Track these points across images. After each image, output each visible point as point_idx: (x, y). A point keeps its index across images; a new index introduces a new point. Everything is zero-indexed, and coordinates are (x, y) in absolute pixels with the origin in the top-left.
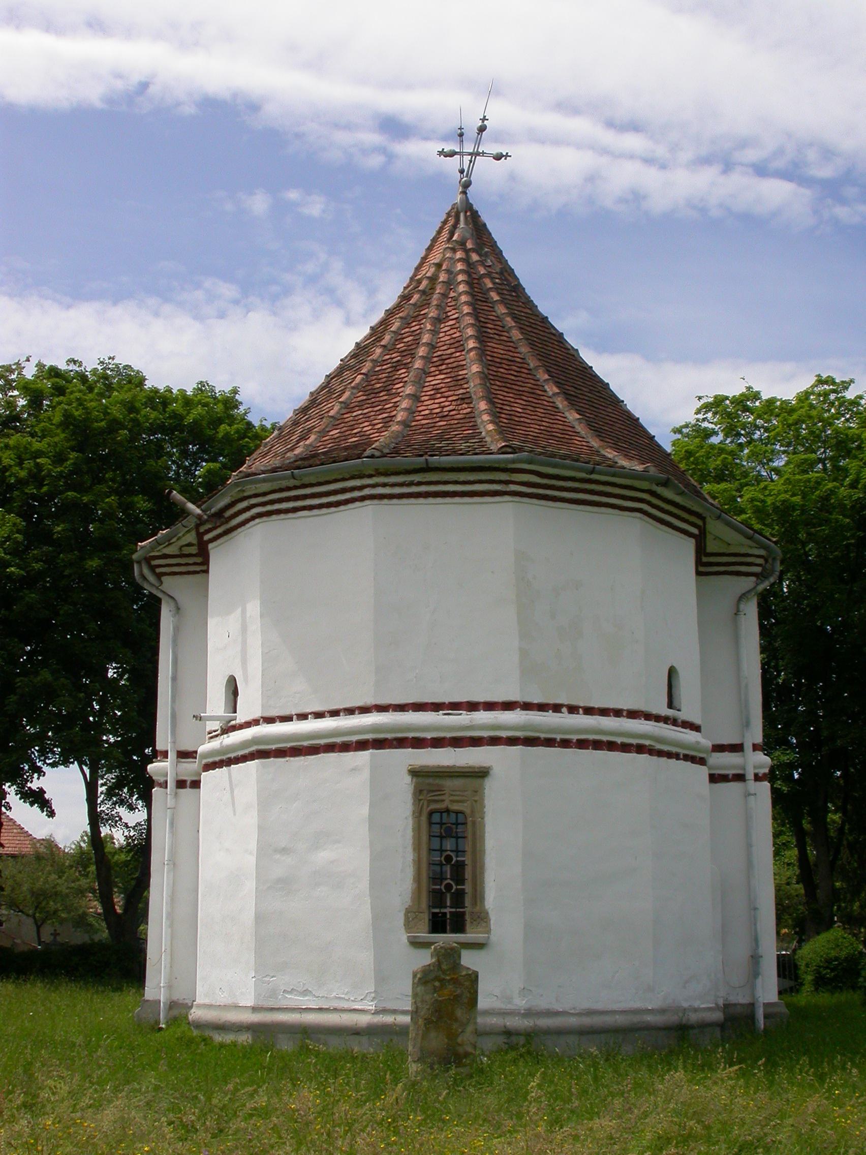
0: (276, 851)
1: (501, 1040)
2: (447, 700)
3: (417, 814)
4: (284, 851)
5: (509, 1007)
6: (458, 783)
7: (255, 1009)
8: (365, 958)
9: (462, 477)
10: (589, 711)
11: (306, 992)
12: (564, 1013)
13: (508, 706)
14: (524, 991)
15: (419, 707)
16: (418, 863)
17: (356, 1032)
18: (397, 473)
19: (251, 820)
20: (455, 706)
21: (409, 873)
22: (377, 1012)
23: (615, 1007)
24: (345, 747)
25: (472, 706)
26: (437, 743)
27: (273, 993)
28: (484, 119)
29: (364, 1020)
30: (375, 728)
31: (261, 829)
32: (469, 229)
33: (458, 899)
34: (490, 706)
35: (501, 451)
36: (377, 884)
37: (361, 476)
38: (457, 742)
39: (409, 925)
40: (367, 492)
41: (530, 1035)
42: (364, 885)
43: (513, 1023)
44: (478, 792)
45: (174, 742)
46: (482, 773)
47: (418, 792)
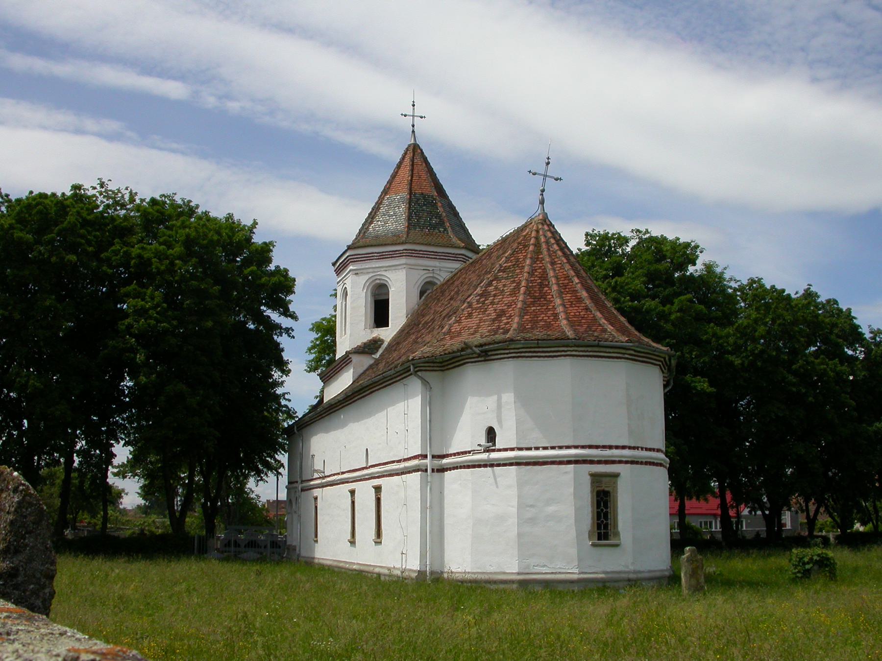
0: (528, 506)
1: (600, 585)
2: (601, 444)
3: (592, 492)
4: (531, 506)
5: (627, 570)
6: (608, 479)
7: (518, 574)
8: (573, 551)
9: (608, 350)
10: (647, 449)
11: (544, 566)
12: (643, 572)
13: (624, 447)
14: (633, 563)
15: (590, 447)
16: (593, 512)
17: (572, 582)
18: (582, 346)
19: (514, 492)
20: (604, 447)
21: (590, 515)
22: (579, 573)
23: (656, 569)
24: (561, 463)
25: (610, 447)
26: (599, 462)
27: (528, 567)
28: (548, 158)
29: (575, 577)
30: (576, 456)
31: (519, 497)
32: (415, 154)
33: (606, 527)
34: (617, 447)
35: (627, 342)
36: (577, 520)
37: (567, 346)
38: (606, 462)
39: (590, 538)
40: (568, 353)
41: (603, 581)
42: (572, 521)
43: (632, 576)
44: (615, 483)
45: (431, 451)
46: (616, 476)
47: (593, 483)
